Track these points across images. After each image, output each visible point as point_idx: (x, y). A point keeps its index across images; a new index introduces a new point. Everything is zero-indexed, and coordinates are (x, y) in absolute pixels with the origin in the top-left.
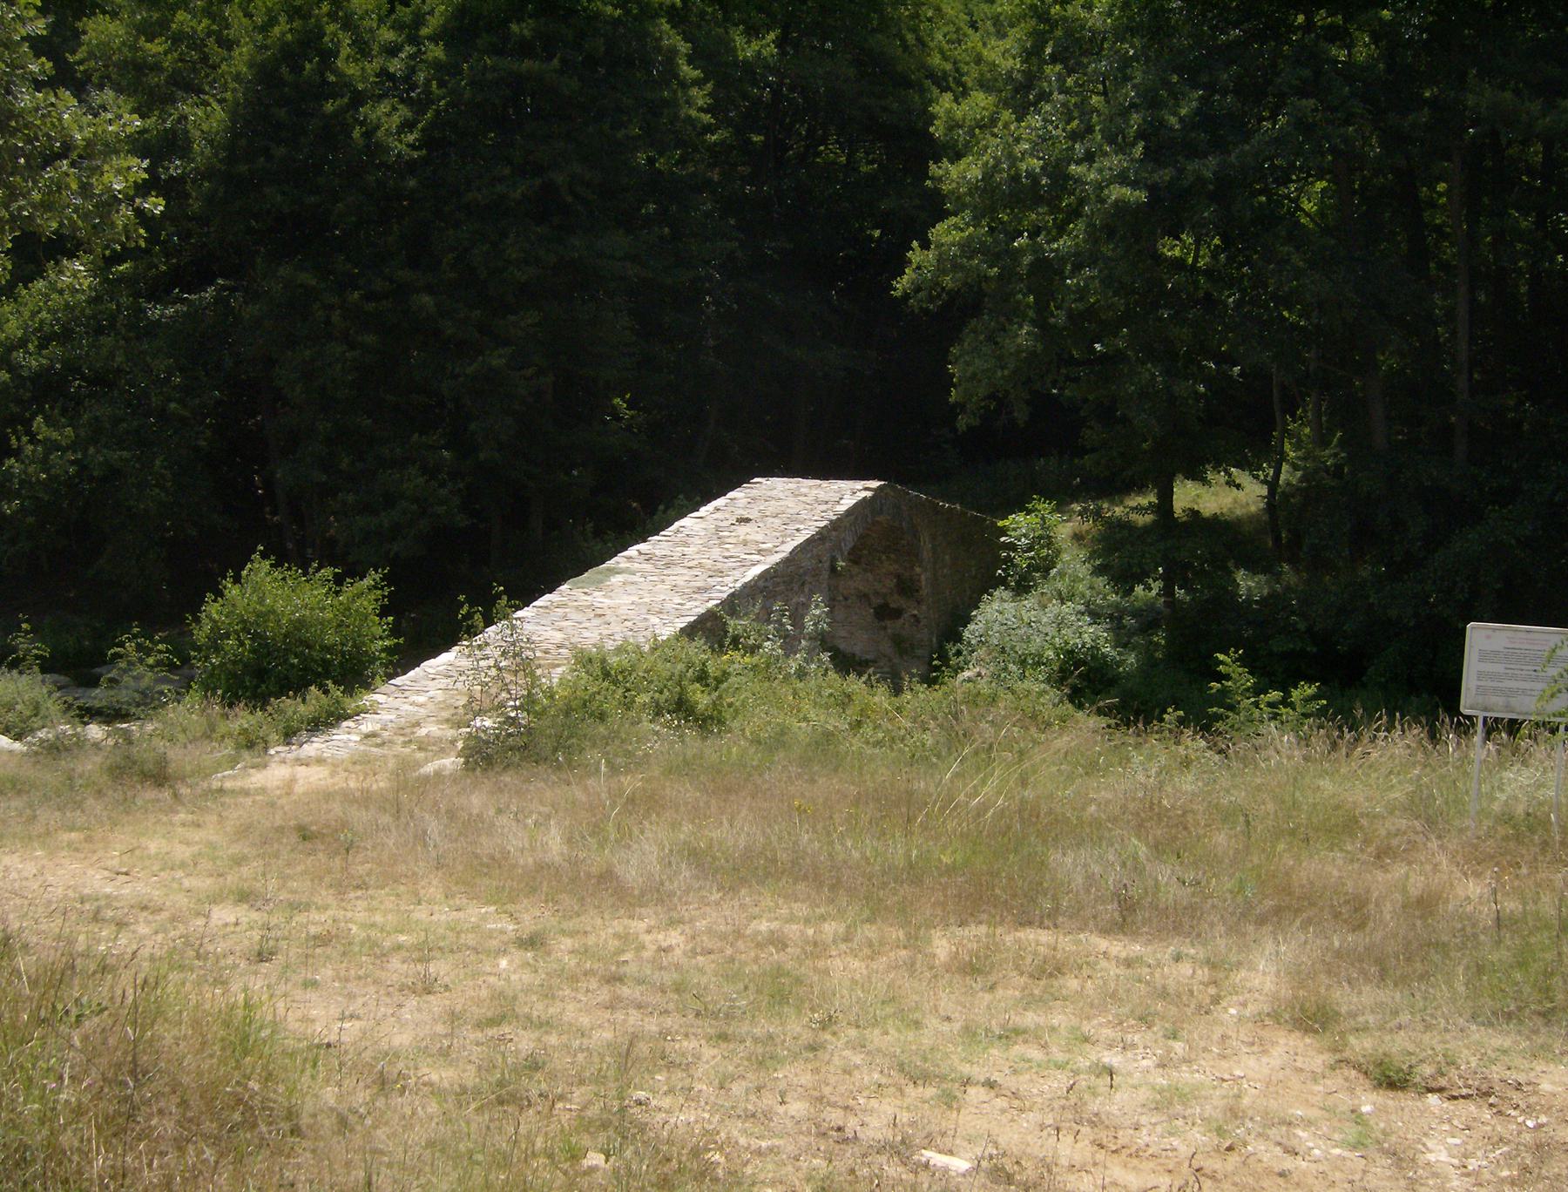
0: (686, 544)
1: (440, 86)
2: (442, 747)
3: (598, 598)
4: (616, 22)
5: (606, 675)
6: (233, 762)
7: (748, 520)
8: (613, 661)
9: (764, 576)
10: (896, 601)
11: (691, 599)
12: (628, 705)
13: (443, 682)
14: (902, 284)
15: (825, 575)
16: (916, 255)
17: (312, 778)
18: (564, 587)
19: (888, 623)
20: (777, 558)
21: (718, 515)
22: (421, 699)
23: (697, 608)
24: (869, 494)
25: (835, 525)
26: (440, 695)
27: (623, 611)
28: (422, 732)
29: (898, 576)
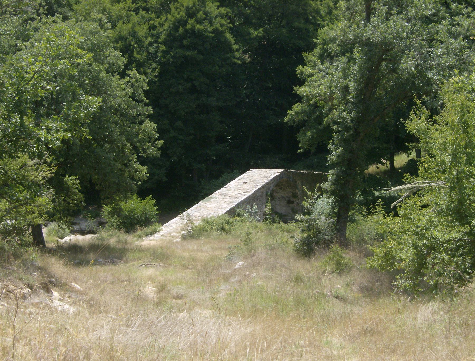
0: (230, 190)
1: (164, 58)
2: (177, 237)
3: (208, 205)
4: (213, 37)
5: (208, 223)
6: (137, 240)
7: (246, 183)
8: (209, 220)
9: (246, 198)
10: (292, 199)
11: (229, 205)
12: (212, 228)
13: (175, 224)
14: (286, 119)
15: (265, 196)
16: (289, 112)
17: (153, 243)
18: (201, 202)
19: (290, 205)
20: (250, 194)
21: (239, 181)
22: (171, 228)
23: (230, 207)
24: (278, 174)
25: (267, 184)
26: (175, 227)
27: (213, 208)
28: (172, 234)
29: (292, 193)
